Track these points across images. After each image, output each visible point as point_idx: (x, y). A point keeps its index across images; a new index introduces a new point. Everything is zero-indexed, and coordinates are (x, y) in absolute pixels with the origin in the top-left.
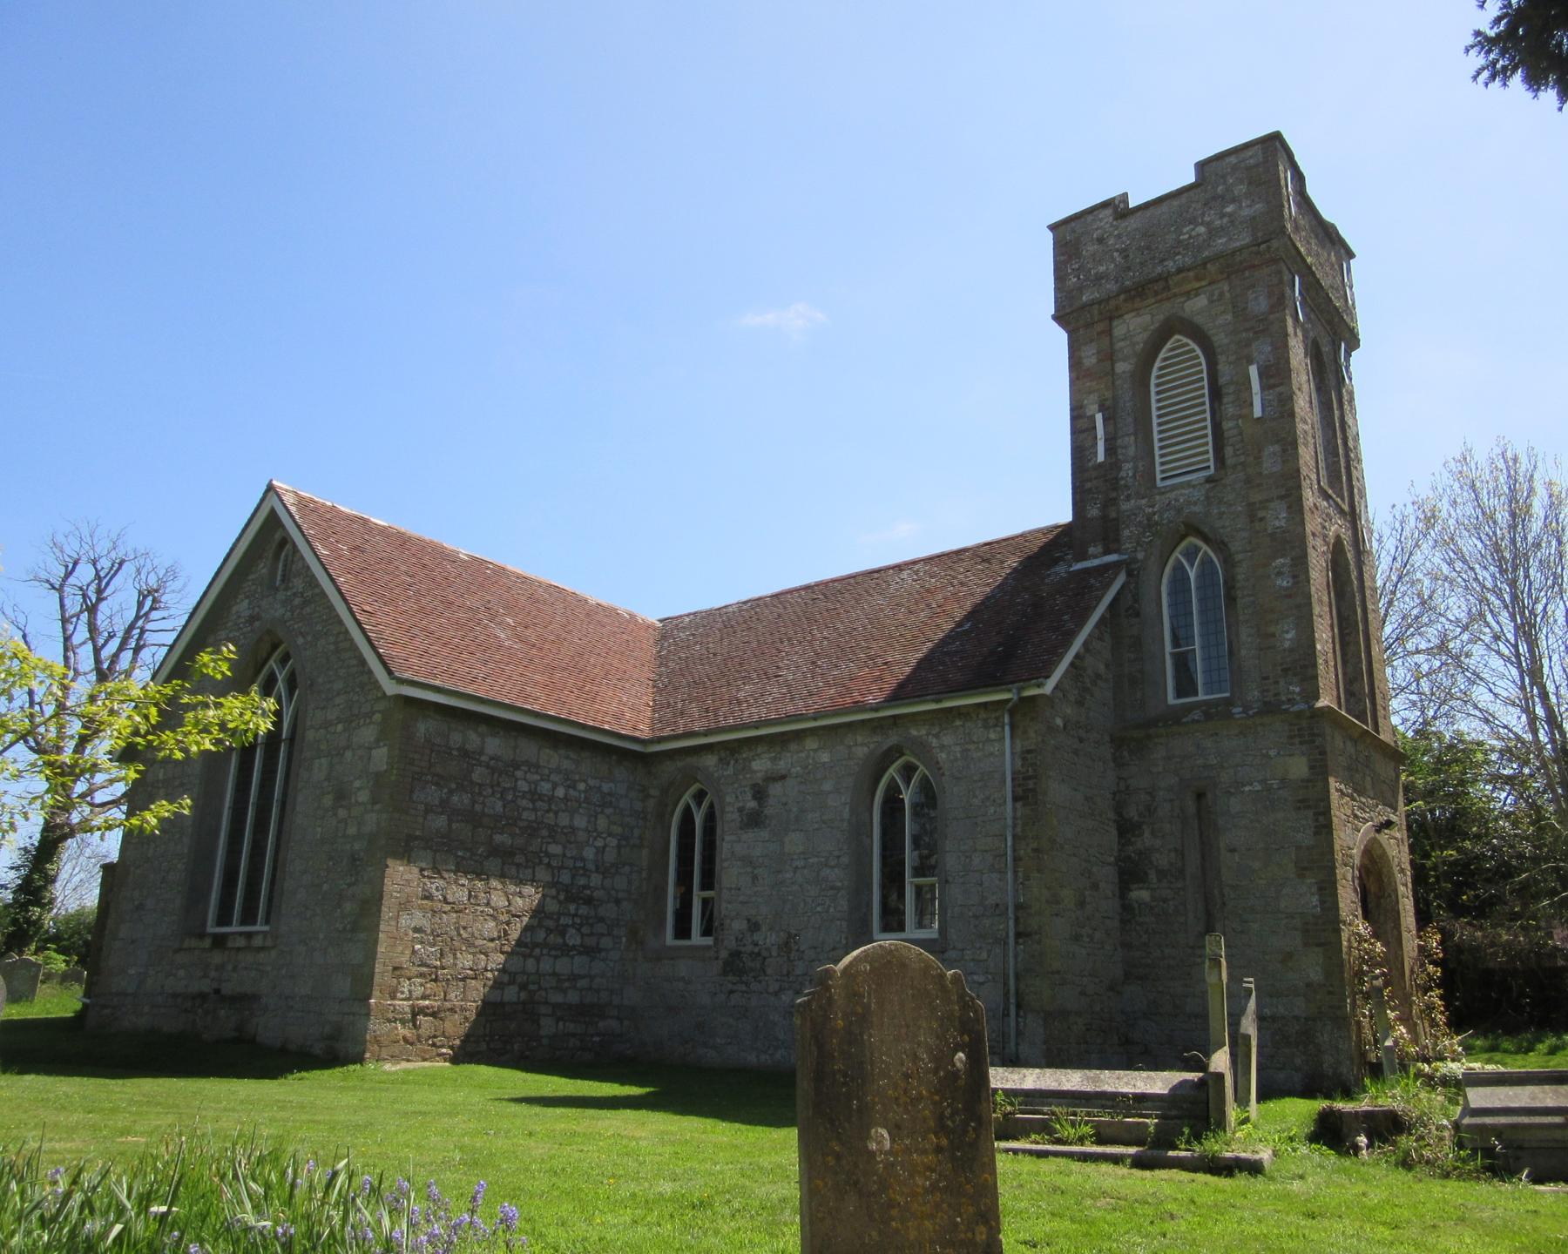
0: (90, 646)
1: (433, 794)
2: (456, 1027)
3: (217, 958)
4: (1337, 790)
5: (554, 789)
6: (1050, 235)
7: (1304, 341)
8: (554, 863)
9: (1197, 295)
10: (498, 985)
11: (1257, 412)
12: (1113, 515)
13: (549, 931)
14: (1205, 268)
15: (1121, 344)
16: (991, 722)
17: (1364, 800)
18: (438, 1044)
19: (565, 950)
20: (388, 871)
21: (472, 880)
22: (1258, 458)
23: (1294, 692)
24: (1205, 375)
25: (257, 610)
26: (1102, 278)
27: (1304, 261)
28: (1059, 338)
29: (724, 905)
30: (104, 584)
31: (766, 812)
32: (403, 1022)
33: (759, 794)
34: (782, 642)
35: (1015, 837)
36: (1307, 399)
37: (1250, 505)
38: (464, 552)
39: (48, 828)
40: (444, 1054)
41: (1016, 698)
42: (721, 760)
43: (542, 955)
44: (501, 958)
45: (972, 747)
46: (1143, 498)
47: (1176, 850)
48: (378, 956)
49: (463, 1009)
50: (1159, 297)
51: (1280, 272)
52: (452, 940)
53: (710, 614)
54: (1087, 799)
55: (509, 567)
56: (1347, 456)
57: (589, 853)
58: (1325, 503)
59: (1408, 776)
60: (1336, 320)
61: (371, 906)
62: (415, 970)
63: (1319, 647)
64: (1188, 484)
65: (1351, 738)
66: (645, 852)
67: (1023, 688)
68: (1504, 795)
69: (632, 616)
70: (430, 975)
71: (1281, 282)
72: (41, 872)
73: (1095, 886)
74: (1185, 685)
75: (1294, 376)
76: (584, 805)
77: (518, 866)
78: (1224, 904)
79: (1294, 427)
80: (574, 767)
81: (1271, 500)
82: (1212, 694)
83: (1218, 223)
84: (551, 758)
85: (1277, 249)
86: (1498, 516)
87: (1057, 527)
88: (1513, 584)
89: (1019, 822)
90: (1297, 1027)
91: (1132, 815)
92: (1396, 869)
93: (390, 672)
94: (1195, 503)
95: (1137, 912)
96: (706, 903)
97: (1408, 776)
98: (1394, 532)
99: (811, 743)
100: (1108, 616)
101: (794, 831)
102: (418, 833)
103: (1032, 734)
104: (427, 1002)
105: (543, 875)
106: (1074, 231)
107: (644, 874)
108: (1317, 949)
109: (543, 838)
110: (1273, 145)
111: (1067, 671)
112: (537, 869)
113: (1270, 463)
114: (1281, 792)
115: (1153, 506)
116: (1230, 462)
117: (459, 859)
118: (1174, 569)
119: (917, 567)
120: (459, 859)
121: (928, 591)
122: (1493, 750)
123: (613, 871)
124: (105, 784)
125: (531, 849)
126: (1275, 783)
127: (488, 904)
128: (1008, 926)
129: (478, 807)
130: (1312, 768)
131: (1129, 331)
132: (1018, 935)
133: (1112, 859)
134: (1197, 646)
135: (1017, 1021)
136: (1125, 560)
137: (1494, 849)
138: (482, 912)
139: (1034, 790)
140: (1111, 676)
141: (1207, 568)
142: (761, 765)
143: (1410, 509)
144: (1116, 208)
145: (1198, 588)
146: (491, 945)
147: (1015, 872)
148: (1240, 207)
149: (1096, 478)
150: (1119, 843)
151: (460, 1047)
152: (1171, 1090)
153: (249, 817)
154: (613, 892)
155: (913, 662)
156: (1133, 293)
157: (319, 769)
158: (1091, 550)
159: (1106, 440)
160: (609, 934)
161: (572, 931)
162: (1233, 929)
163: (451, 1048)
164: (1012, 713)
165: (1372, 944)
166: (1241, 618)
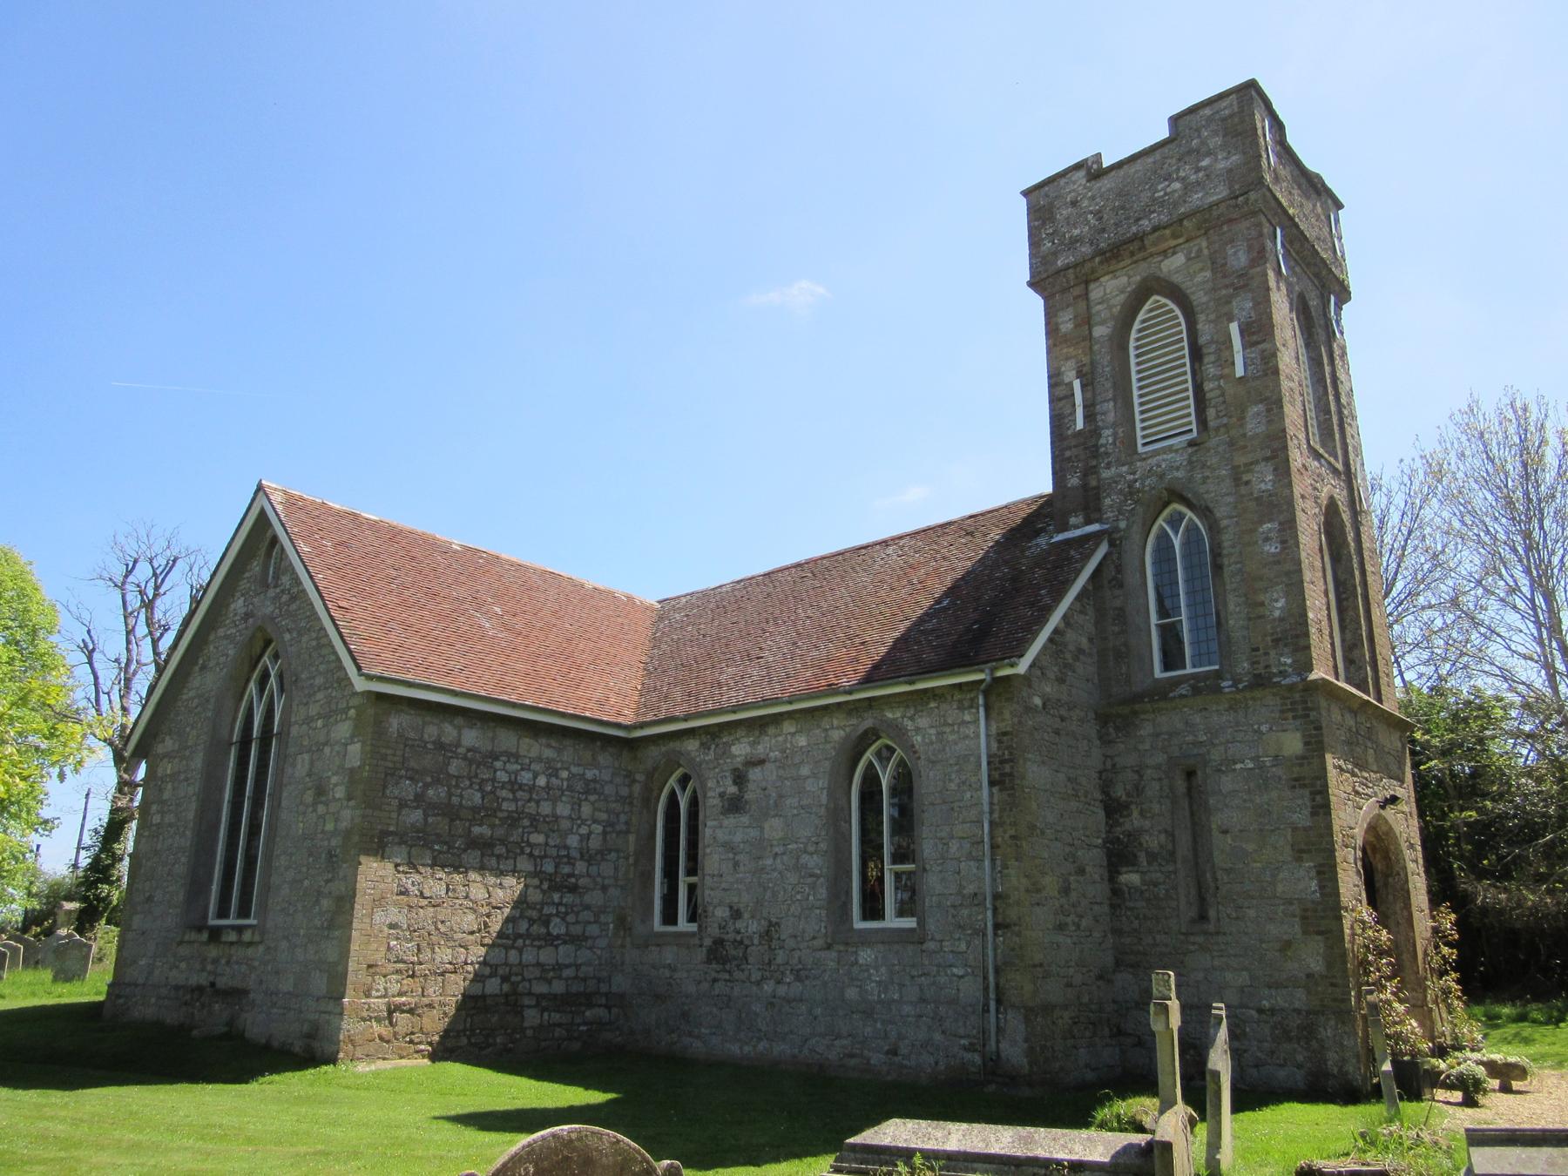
0: (149, 639)
1: (408, 789)
2: (435, 1023)
3: (213, 952)
4: (1335, 767)
5: (535, 778)
6: (1023, 202)
7: (1288, 296)
8: (536, 853)
9: (1174, 253)
10: (478, 978)
11: (1239, 371)
12: (1094, 483)
13: (532, 921)
14: (1181, 225)
15: (1099, 307)
16: (966, 704)
17: (1366, 775)
18: (416, 1040)
19: (550, 940)
20: (361, 868)
21: (450, 873)
22: (1242, 418)
23: (1285, 664)
24: (1184, 335)
25: (251, 606)
26: (1077, 241)
27: (1285, 212)
28: (1035, 304)
29: (707, 892)
30: (160, 581)
31: (746, 797)
32: (379, 1020)
33: (740, 778)
34: (767, 622)
35: (991, 823)
36: (1293, 354)
37: (1235, 468)
38: (457, 542)
39: (114, 811)
40: (422, 1051)
41: (989, 679)
42: (702, 744)
43: (525, 945)
44: (482, 951)
45: (948, 730)
46: (1123, 465)
47: (1166, 831)
48: (352, 953)
49: (442, 1004)
50: (1135, 258)
51: (1259, 225)
52: (429, 934)
53: (705, 595)
54: (1069, 779)
55: (504, 556)
56: (1340, 413)
57: (573, 841)
58: (1316, 463)
59: (1423, 734)
60: (1324, 272)
61: (345, 902)
62: (391, 967)
63: (1311, 615)
64: (1170, 449)
65: (1351, 711)
66: (632, 838)
67: (996, 668)
68: (1525, 752)
69: (630, 598)
70: (407, 971)
71: (1261, 235)
72: (108, 851)
73: (1081, 871)
74: (1172, 658)
75: (1277, 332)
76: (566, 793)
77: (499, 857)
78: (1217, 888)
79: (1278, 385)
80: (556, 755)
81: (1257, 462)
82: (1201, 666)
83: (1193, 178)
84: (531, 748)
85: (1256, 201)
86: (1509, 467)
87: (1041, 497)
88: (1527, 535)
89: (996, 807)
90: (1299, 1022)
91: (1119, 794)
92: (1404, 846)
93: (359, 668)
94: (1178, 469)
95: (1127, 895)
96: (692, 888)
97: (1423, 734)
98: (1403, 486)
99: (789, 727)
100: (1090, 588)
101: (774, 816)
102: (392, 829)
103: (1007, 715)
104: (404, 999)
105: (525, 864)
106: (1047, 196)
107: (631, 860)
108: (1319, 938)
109: (524, 828)
110: (1250, 92)
111: (1045, 647)
112: (519, 858)
113: (1254, 424)
114: (1274, 769)
115: (1134, 473)
116: (1212, 424)
117: (436, 853)
118: (1158, 538)
120: (436, 853)
121: (911, 567)
122: (1511, 705)
123: (599, 857)
125: (512, 839)
128: (985, 918)
129: (455, 800)
130: (1306, 744)
131: (1105, 294)
132: (997, 926)
133: (1100, 841)
134: (1184, 617)
135: (997, 1018)
136: (1107, 529)
137: (1516, 807)
138: (461, 905)
139: (1011, 775)
140: (1095, 650)
142: (741, 749)
143: (1419, 463)
144: (1089, 169)
145: (1184, 557)
146: (471, 937)
147: (993, 860)
148: (1216, 160)
149: (1075, 446)
150: (1107, 823)
151: (439, 1043)
152: (1113, 1157)
153: (224, 813)
154: (599, 879)
155: (890, 642)
156: (1108, 255)
157: (302, 765)
158: (1073, 520)
159: (1084, 407)
160: (595, 922)
161: (557, 920)
162: (1228, 916)
163: (430, 1044)
164: (986, 693)
165: (1378, 931)
166: (1228, 587)
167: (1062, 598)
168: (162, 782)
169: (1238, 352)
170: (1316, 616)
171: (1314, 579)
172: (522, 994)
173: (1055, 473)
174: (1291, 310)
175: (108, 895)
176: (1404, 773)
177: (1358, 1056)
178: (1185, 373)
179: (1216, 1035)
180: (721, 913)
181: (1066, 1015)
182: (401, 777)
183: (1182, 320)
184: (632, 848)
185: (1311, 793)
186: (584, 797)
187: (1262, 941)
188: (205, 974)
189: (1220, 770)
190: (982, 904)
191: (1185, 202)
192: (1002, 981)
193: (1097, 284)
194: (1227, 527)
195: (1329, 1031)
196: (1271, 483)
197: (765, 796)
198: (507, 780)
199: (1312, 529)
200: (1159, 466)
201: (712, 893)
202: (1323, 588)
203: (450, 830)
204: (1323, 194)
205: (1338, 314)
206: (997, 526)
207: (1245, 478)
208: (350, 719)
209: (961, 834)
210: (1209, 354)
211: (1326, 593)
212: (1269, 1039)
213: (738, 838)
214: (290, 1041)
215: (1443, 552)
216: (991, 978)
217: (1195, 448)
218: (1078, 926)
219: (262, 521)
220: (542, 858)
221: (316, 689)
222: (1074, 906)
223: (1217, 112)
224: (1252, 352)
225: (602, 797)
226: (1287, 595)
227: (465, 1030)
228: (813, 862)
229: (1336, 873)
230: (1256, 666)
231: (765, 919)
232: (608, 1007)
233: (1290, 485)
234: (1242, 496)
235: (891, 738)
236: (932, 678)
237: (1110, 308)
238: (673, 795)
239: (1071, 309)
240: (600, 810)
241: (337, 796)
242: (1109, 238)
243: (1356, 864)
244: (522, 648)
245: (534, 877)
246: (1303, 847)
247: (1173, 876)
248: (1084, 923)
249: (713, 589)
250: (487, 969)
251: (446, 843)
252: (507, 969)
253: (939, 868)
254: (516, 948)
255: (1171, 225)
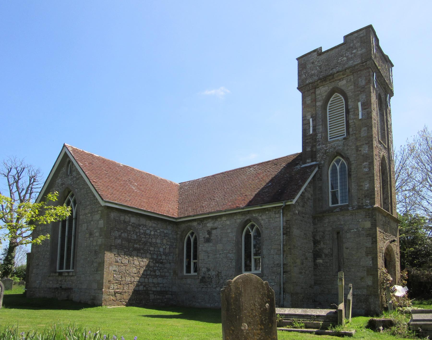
0: (17, 192)
1: (117, 234)
2: (127, 297)
3: (60, 278)
4: (379, 231)
6: (297, 62)
7: (376, 94)
8: (152, 253)
9: (343, 80)
10: (137, 286)
11: (360, 117)
12: (315, 150)
15: (319, 96)
16: (277, 212)
19: (156, 276)
20: (105, 255)
23: (367, 203)
24: (344, 106)
26: (313, 75)
27: (377, 68)
29: (200, 264)
30: (19, 175)
32: (112, 295)
33: (209, 233)
34: (215, 189)
35: (283, 245)
36: (376, 113)
38: (122, 164)
39: (11, 243)
40: (124, 304)
41: (284, 205)
42: (198, 223)
43: (149, 278)
44: (138, 278)
45: (271, 219)
46: (324, 145)
47: (330, 248)
49: (128, 292)
50: (331, 81)
51: (369, 72)
52: (124, 273)
53: (194, 181)
54: (304, 234)
55: (135, 168)
57: (161, 250)
58: (380, 145)
59: (400, 227)
61: (101, 264)
62: (114, 282)
63: (376, 189)
64: (338, 140)
66: (177, 250)
67: (286, 202)
69: (171, 182)
70: (119, 283)
71: (369, 75)
73: (306, 259)
74: (335, 201)
75: (372, 105)
76: (159, 236)
77: (142, 253)
79: (371, 121)
80: (156, 226)
81: (363, 144)
82: (343, 203)
84: (150, 223)
87: (297, 154)
92: (395, 254)
93: (102, 199)
94: (340, 146)
95: (318, 266)
97: (400, 227)
98: (401, 154)
99: (224, 219)
100: (312, 181)
103: (289, 215)
104: (118, 290)
105: (149, 256)
107: (177, 256)
108: (371, 276)
109: (148, 246)
110: (369, 29)
111: (299, 197)
112: (147, 254)
113: (363, 133)
114: (362, 232)
116: (351, 133)
118: (333, 166)
119: (255, 167)
120: (125, 252)
121: (258, 174)
122: (427, 219)
123: (168, 254)
124: (25, 231)
126: (360, 229)
127: (134, 264)
129: (129, 237)
130: (372, 225)
131: (321, 92)
132: (284, 272)
133: (312, 251)
134: (339, 189)
135: (283, 296)
136: (318, 164)
137: (425, 248)
139: (289, 232)
141: (343, 166)
142: (210, 225)
143: (406, 147)
144: (318, 52)
145: (340, 172)
147: (283, 255)
148: (358, 50)
149: (310, 139)
150: (314, 246)
151: (128, 302)
154: (168, 261)
155: (254, 195)
156: (322, 80)
157: (84, 226)
158: (308, 161)
160: (168, 272)
161: (158, 271)
162: (347, 271)
163: (126, 302)
164: (283, 209)
167: (305, 183)
168: (39, 232)
169: (360, 111)
170: (377, 189)
171: (377, 179)
172: (149, 290)
173: (303, 147)
174: (376, 99)
175: (11, 268)
176: (397, 234)
177: (379, 306)
178: (344, 117)
179: (349, 291)
180: (204, 270)
181: (301, 296)
182: (115, 230)
183: (344, 101)
184: (177, 253)
185: (372, 238)
186: (164, 238)
187: (355, 277)
188: (58, 284)
189: (347, 232)
190: (280, 266)
191: (347, 64)
192: (285, 286)
193: (318, 89)
194: (353, 164)
195: (372, 300)
196: (367, 151)
197: (217, 238)
198: (143, 232)
199: (378, 164)
200: (334, 145)
201: (201, 264)
202: (379, 182)
203: (128, 245)
204: (388, 62)
205: (389, 100)
206: (284, 162)
207: (360, 149)
208: (99, 214)
209: (274, 248)
210: (352, 112)
211: (380, 183)
212: (355, 302)
213: (209, 249)
214: (87, 301)
215: (411, 174)
216: (282, 285)
217: (346, 140)
218: (305, 273)
219: (66, 155)
220: (153, 254)
221: (87, 205)
222: (304, 268)
223: (359, 35)
224: (364, 112)
225: (169, 238)
226: (369, 183)
227: (134, 299)
228: (231, 256)
229: (377, 259)
230: (359, 203)
231: (217, 271)
232: (171, 295)
233: (373, 152)
234: (359, 154)
235: (254, 222)
236: (272, 204)
237: (322, 96)
238: (189, 238)
239: (310, 97)
240: (168, 242)
241: (96, 235)
242: (323, 75)
243: (383, 257)
244: (144, 195)
245: (151, 259)
246: (369, 252)
247: (332, 260)
248: (307, 272)
249: (196, 180)
250: (140, 283)
251: (128, 249)
252: (145, 284)
253: (268, 257)
254: (147, 278)
255: (342, 71)
